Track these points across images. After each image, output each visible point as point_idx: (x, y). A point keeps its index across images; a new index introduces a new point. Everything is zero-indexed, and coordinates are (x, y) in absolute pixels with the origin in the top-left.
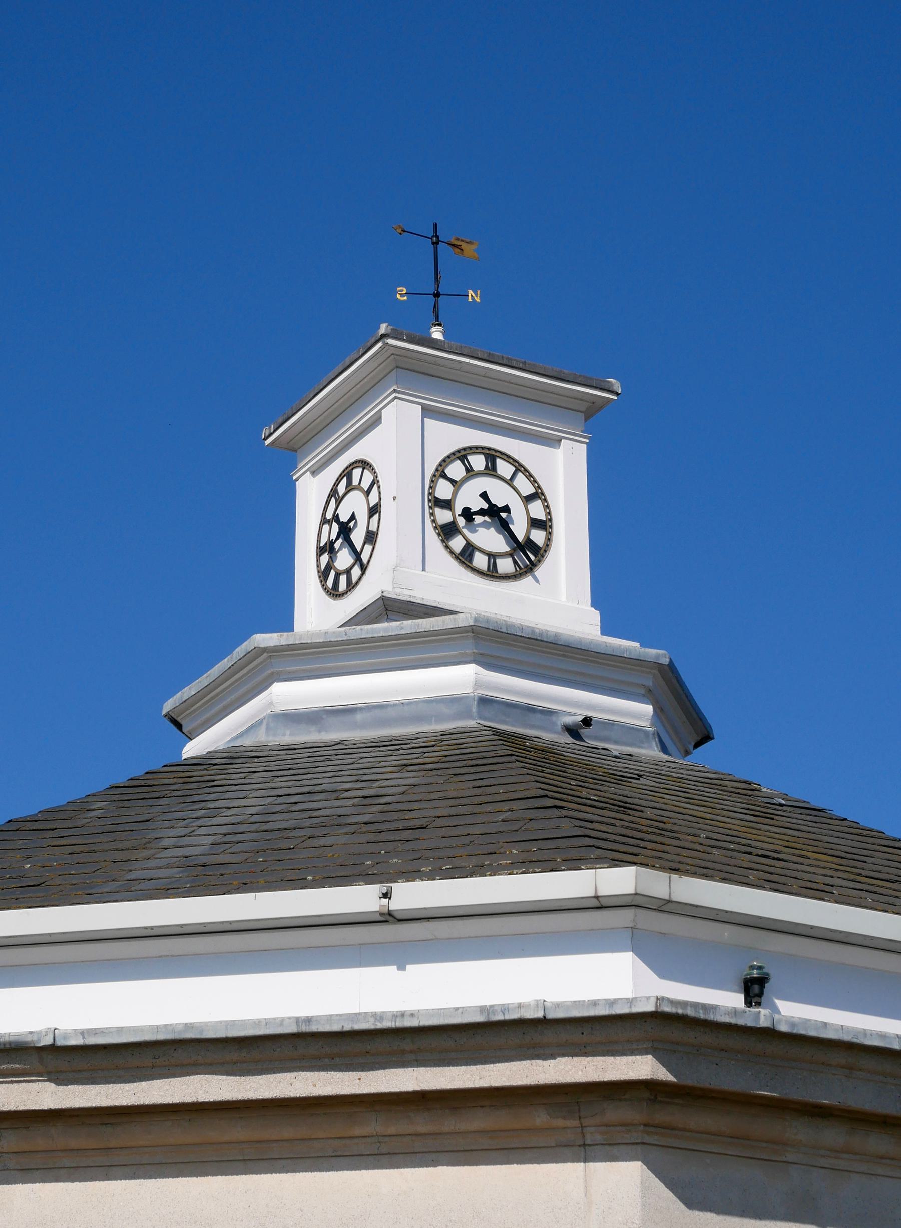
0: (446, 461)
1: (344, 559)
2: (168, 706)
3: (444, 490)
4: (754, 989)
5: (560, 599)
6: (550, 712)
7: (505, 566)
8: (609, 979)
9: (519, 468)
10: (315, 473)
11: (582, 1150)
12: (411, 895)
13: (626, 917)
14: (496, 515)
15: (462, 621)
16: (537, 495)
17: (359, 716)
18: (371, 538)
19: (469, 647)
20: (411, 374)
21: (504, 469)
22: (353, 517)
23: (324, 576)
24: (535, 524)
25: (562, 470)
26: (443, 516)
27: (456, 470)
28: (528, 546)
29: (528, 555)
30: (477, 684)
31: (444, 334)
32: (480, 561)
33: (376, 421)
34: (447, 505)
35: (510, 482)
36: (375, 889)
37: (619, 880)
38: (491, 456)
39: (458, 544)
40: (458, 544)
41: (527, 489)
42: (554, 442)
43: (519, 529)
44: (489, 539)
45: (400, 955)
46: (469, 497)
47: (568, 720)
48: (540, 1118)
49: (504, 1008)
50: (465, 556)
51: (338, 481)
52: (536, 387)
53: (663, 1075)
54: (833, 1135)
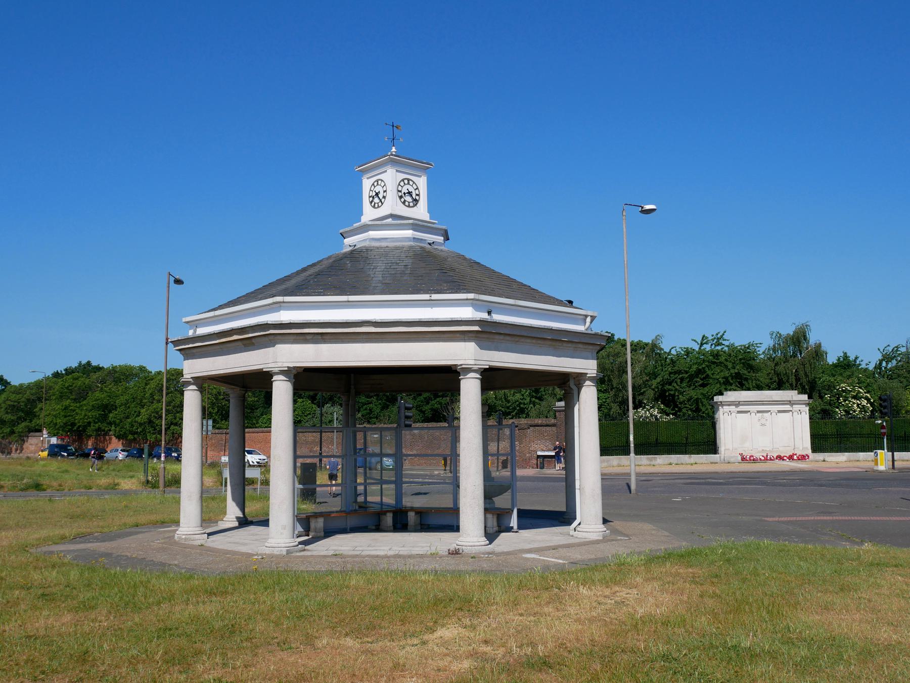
1: (376, 200)
2: (341, 231)
3: (400, 188)
4: (489, 313)
7: (411, 204)
8: (467, 313)
11: (465, 341)
12: (435, 296)
14: (410, 193)
18: (384, 197)
20: (393, 162)
21: (411, 183)
23: (371, 202)
24: (418, 195)
25: (422, 182)
26: (400, 194)
27: (402, 184)
29: (416, 201)
32: (407, 203)
37: (471, 296)
38: (409, 180)
43: (414, 196)
45: (432, 306)
46: (405, 190)
48: (458, 335)
50: (404, 203)
54: (502, 337)
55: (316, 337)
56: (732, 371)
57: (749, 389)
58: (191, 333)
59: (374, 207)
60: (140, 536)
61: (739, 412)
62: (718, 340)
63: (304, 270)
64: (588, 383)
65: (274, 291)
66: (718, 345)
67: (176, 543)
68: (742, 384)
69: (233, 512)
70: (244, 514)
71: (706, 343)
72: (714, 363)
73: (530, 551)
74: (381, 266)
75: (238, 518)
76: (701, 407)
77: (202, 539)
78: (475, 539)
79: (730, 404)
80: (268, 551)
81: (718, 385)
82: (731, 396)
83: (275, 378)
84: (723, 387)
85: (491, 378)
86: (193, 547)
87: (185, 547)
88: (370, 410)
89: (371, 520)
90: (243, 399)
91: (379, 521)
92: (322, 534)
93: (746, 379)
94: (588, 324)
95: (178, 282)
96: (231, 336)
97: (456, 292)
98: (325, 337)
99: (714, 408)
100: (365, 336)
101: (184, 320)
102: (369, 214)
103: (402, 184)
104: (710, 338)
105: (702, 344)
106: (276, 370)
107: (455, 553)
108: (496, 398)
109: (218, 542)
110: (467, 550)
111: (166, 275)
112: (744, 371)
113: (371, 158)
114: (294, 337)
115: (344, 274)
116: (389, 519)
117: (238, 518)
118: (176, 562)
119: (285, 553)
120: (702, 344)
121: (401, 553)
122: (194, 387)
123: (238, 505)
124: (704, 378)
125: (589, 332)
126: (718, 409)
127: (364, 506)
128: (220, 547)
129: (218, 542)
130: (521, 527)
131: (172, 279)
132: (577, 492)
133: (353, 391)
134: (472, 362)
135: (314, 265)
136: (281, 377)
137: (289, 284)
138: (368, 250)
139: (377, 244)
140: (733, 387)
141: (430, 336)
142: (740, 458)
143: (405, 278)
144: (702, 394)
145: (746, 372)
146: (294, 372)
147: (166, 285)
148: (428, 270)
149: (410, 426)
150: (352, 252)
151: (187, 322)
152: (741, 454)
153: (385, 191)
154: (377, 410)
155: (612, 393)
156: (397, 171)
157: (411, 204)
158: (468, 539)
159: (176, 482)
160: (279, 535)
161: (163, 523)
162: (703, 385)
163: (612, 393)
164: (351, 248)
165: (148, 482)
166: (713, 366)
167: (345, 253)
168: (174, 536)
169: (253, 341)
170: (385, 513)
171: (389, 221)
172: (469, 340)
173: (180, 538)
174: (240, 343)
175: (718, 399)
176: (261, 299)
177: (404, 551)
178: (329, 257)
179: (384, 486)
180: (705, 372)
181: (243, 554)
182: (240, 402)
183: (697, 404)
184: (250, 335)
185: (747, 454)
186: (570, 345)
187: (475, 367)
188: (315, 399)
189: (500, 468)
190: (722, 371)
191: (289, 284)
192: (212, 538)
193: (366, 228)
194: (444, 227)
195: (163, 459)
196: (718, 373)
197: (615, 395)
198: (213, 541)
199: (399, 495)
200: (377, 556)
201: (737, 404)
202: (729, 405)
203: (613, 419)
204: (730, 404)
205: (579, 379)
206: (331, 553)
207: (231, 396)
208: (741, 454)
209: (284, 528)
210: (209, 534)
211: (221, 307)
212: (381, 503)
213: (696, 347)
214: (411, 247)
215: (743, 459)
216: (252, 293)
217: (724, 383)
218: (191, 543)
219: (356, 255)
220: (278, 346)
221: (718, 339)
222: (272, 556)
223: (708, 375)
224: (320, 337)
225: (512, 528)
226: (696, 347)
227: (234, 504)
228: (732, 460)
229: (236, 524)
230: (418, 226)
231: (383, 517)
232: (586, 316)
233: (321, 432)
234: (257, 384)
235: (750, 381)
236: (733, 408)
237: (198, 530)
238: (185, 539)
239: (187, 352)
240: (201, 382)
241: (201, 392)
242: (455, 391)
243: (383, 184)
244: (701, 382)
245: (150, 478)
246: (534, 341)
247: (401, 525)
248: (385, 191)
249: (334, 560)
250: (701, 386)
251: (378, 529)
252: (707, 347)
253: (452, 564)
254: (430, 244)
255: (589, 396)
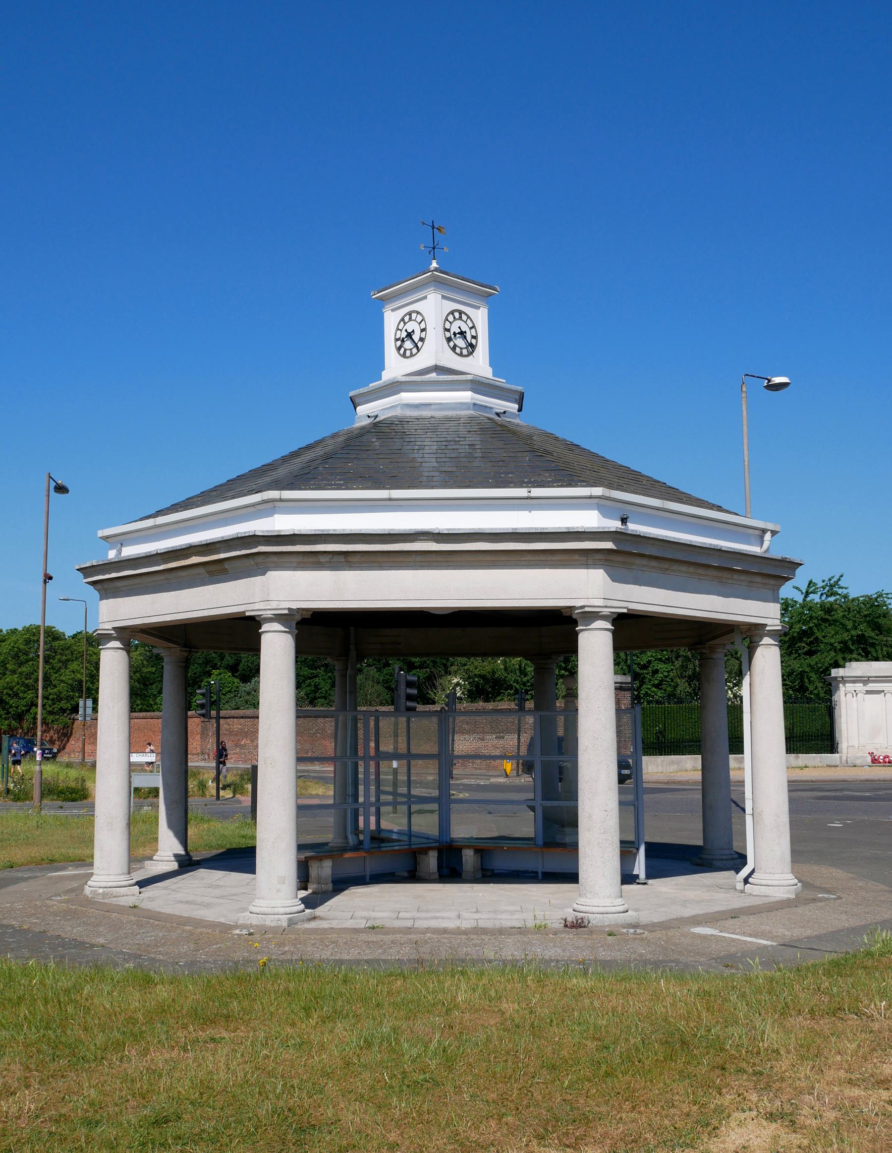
0: (448, 315)
1: (408, 344)
2: (352, 394)
3: (448, 326)
4: (624, 521)
5: (479, 364)
6: (491, 408)
7: (465, 352)
8: (589, 519)
9: (468, 317)
10: (393, 310)
11: (587, 566)
12: (537, 492)
13: (597, 501)
14: (462, 334)
15: (469, 377)
16: (473, 327)
17: (433, 407)
19: (469, 386)
20: (438, 283)
21: (464, 317)
22: (413, 331)
23: (399, 349)
24: (473, 337)
25: (480, 316)
26: (448, 334)
28: (471, 345)
29: (472, 347)
30: (472, 399)
31: (437, 263)
33: (425, 297)
34: (449, 330)
35: (466, 322)
36: (526, 490)
37: (598, 491)
38: (461, 312)
39: (452, 344)
40: (452, 344)
41: (471, 325)
42: (478, 308)
44: (460, 342)
45: (530, 508)
46: (455, 328)
47: (498, 411)
48: (576, 557)
49: (573, 528)
50: (453, 349)
51: (405, 315)
52: (479, 290)
53: (614, 548)
54: (644, 562)
55: (336, 559)
56: (854, 633)
57: (877, 659)
58: (112, 555)
59: (404, 356)
60: (23, 886)
61: (868, 692)
62: (832, 587)
63: (295, 455)
64: (767, 640)
65: (261, 481)
66: (832, 595)
67: (89, 902)
68: (867, 650)
69: (168, 847)
70: (186, 848)
71: (814, 592)
72: (825, 620)
73: (696, 920)
74: (430, 446)
75: (177, 856)
76: (807, 684)
77: (131, 896)
78: (608, 902)
79: (856, 680)
80: (255, 920)
81: (833, 654)
82: (857, 668)
83: (265, 627)
84: (840, 656)
85: (630, 629)
86: (120, 910)
87: (105, 910)
88: (316, 686)
89: (405, 863)
90: (186, 664)
91: (416, 863)
92: (330, 887)
93: (873, 645)
94: (766, 544)
95: (61, 489)
96: (187, 557)
97: (569, 485)
98: (351, 559)
99: (830, 687)
100: (419, 558)
101: (101, 533)
102: (395, 367)
103: (451, 318)
104: (820, 584)
105: (807, 594)
106: (268, 614)
107: (577, 925)
108: (506, 669)
109: (158, 899)
110: (595, 920)
111: (46, 478)
112: (870, 633)
113: (397, 274)
114: (300, 559)
115: (371, 457)
116: (432, 861)
117: (177, 856)
118: (101, 941)
119: (285, 924)
120: (807, 594)
121: (482, 924)
122: (117, 644)
123: (177, 835)
124: (811, 643)
125: (766, 555)
126: (838, 688)
127: (379, 838)
128: (168, 910)
129: (158, 899)
130: (653, 873)
131: (53, 484)
132: (749, 819)
133: (353, 654)
134: (600, 603)
135: (309, 447)
136: (277, 626)
137: (282, 472)
138: (402, 421)
139: (409, 413)
140: (855, 656)
141: (529, 557)
142: (869, 759)
143: (476, 464)
144: (810, 665)
145: (873, 634)
146: (298, 618)
147: (45, 493)
148: (506, 453)
149: (413, 709)
150: (375, 425)
151: (102, 538)
152: (871, 754)
153: (423, 330)
154: (325, 687)
155: (678, 663)
156: (444, 297)
157: (465, 352)
158: (595, 902)
159: (78, 795)
160: (270, 892)
161: (52, 861)
162: (810, 653)
163: (678, 663)
164: (369, 421)
165: (8, 791)
166: (823, 625)
167: (363, 428)
168: (81, 888)
169: (227, 565)
170: (425, 851)
171: (433, 376)
172: (594, 566)
173: (94, 892)
174: (201, 570)
175: (834, 672)
176: (233, 497)
177: (486, 920)
178: (334, 436)
179: (414, 808)
180: (813, 634)
181: (213, 925)
182: (197, 669)
183: (802, 681)
184: (222, 556)
185: (880, 754)
186: (743, 577)
187: (606, 611)
188: (237, 671)
189: (520, 773)
190: (837, 633)
191: (282, 472)
192: (151, 891)
193: (395, 387)
194: (520, 388)
195: (38, 758)
196: (831, 636)
197: (682, 666)
198: (152, 899)
199: (444, 823)
200: (445, 931)
201: (866, 680)
202: (854, 682)
203: (680, 701)
204: (856, 680)
205: (750, 634)
206: (362, 924)
207: (165, 660)
208: (871, 754)
209: (282, 881)
210: (142, 884)
211: (141, 519)
212: (410, 834)
213: (800, 598)
214: (471, 418)
215: (875, 761)
216: (211, 491)
217: (841, 650)
218: (114, 901)
219: (379, 428)
220: (271, 574)
221: (831, 586)
222: (265, 930)
223: (816, 639)
224: (341, 559)
225: (637, 876)
226: (800, 598)
227: (171, 834)
228: (858, 762)
229: (174, 866)
230: (478, 385)
231: (421, 858)
232: (764, 531)
233: (218, 718)
234: (237, 637)
235: (878, 648)
236: (859, 686)
237: (123, 880)
238: (104, 894)
239: (106, 586)
240: (127, 635)
241: (128, 652)
242: (571, 649)
243: (419, 318)
244: (807, 648)
245: (11, 786)
246: (692, 569)
247: (450, 872)
248: (423, 330)
249: (373, 937)
250: (805, 654)
251: (413, 876)
252: (815, 598)
253: (573, 948)
254: (498, 414)
255: (768, 661)
